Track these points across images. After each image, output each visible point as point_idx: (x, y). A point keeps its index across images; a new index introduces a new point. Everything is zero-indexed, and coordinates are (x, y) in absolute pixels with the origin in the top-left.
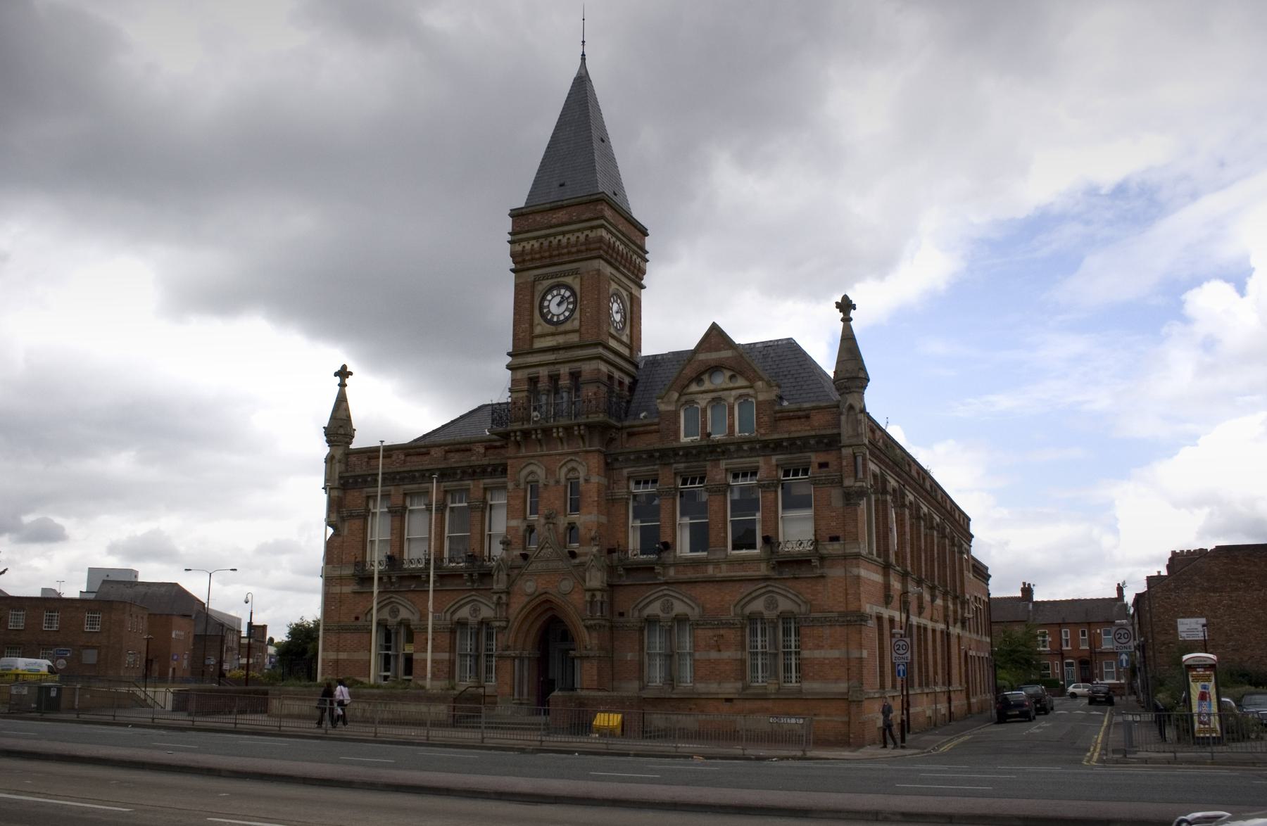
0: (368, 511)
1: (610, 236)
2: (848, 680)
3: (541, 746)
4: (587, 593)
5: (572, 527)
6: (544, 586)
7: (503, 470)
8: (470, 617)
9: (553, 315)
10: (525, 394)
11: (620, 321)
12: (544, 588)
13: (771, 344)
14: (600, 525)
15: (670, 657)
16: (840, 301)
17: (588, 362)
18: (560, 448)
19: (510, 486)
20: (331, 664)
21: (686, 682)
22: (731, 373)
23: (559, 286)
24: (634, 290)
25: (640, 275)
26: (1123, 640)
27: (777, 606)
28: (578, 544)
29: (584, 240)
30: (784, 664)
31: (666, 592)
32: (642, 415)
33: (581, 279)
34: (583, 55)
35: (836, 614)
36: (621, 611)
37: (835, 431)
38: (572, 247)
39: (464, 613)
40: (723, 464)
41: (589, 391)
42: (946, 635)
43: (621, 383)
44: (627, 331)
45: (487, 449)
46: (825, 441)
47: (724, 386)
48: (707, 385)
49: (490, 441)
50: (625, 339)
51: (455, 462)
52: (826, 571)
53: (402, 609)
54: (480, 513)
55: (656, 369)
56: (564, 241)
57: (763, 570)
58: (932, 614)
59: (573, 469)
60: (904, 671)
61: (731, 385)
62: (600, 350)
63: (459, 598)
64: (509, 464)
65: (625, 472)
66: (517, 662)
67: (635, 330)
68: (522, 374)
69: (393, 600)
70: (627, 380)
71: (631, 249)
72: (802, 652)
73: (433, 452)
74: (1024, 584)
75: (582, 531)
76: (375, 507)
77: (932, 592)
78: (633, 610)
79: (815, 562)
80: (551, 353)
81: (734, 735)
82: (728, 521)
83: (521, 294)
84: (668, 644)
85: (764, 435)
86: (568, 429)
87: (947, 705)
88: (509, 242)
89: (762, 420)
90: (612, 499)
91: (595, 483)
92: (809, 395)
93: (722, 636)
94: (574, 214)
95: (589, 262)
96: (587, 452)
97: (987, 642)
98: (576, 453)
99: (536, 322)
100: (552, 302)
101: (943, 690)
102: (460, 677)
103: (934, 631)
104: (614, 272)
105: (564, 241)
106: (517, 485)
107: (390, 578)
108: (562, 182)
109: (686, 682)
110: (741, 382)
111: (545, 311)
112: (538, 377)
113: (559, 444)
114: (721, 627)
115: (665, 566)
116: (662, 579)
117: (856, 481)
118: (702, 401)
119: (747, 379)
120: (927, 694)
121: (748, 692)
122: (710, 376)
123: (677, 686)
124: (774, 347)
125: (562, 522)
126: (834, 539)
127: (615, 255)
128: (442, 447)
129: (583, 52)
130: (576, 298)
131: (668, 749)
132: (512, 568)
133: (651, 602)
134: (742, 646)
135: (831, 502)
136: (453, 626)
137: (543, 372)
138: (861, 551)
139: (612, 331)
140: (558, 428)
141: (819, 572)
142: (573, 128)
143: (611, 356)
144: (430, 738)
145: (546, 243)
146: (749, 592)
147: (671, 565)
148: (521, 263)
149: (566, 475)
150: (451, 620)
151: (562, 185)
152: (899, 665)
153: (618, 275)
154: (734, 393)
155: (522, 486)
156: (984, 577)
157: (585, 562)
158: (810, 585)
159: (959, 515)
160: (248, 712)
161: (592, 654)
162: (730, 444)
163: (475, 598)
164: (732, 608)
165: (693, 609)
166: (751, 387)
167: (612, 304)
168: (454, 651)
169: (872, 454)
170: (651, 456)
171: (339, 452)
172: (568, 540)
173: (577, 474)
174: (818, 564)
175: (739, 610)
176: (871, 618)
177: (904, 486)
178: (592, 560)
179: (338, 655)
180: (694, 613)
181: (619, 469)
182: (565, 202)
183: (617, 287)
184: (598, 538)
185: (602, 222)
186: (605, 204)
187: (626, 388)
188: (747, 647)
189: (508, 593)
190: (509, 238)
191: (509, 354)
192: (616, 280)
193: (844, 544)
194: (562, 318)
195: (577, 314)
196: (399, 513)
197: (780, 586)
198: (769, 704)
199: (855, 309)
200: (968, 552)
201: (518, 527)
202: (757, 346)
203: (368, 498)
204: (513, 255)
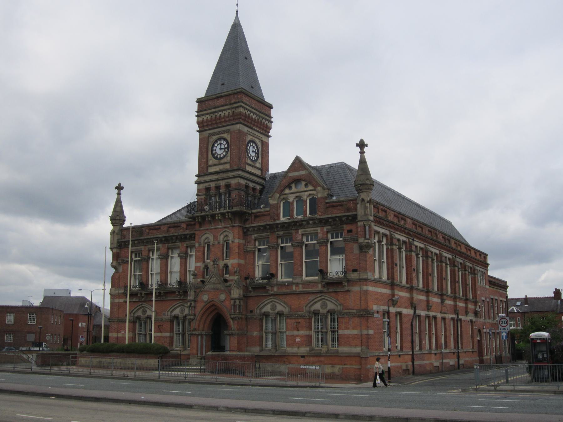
0: (149, 258)
3: (32, 371)
5: (226, 266)
6: (212, 297)
7: (192, 237)
8: (180, 314)
9: (218, 154)
11: (255, 156)
12: (212, 298)
13: (332, 165)
16: (359, 143)
17: (234, 179)
18: (220, 225)
19: (197, 245)
20: (114, 339)
22: (306, 183)
23: (221, 139)
24: (264, 138)
25: (268, 130)
26: (504, 325)
27: (327, 306)
28: (228, 275)
29: (232, 114)
31: (273, 300)
32: (262, 206)
33: (231, 135)
34: (237, 12)
35: (355, 311)
36: (251, 310)
37: (354, 213)
38: (226, 118)
39: (177, 312)
40: (300, 232)
41: (234, 194)
42: (457, 322)
43: (254, 189)
44: (260, 160)
45: (187, 225)
46: (350, 218)
47: (302, 190)
48: (294, 189)
55: (275, 180)
56: (223, 115)
57: (320, 287)
59: (227, 236)
61: (305, 189)
62: (240, 173)
63: (174, 304)
64: (196, 234)
65: (253, 236)
66: (199, 337)
67: (264, 160)
68: (202, 186)
69: (143, 305)
70: (258, 187)
71: (260, 117)
72: (339, 331)
74: (556, 289)
75: (230, 267)
76: (153, 255)
78: (257, 309)
80: (216, 175)
81: (306, 375)
84: (274, 327)
86: (223, 215)
87: (456, 360)
88: (196, 116)
90: (247, 251)
91: (237, 243)
92: (346, 193)
93: (300, 322)
94: (228, 100)
96: (233, 227)
98: (228, 227)
100: (217, 147)
101: (453, 351)
102: (176, 345)
103: (444, 319)
104: (249, 130)
105: (223, 115)
106: (200, 245)
107: (141, 294)
108: (223, 82)
111: (214, 152)
113: (220, 223)
114: (299, 318)
115: (272, 286)
116: (270, 293)
117: (365, 240)
119: (313, 185)
120: (435, 354)
123: (279, 349)
124: (333, 167)
125: (221, 263)
126: (355, 271)
128: (166, 225)
129: (237, 10)
130: (229, 145)
131: (246, 381)
132: (197, 288)
133: (266, 305)
136: (172, 319)
137: (213, 185)
139: (249, 162)
141: (347, 288)
142: (230, 53)
143: (247, 175)
144: (136, 376)
145: (214, 116)
146: (312, 299)
147: (275, 285)
148: (203, 126)
149: (223, 239)
150: (171, 316)
151: (223, 84)
153: (252, 131)
154: (307, 193)
155: (202, 245)
156: (503, 288)
157: (231, 285)
160: (186, 365)
161: (234, 332)
164: (304, 308)
165: (285, 308)
166: (315, 190)
167: (249, 147)
168: (173, 332)
170: (264, 228)
171: (118, 228)
172: (224, 272)
173: (228, 239)
175: (308, 308)
178: (234, 284)
179: (117, 335)
180: (286, 310)
181: (250, 235)
182: (223, 94)
184: (238, 272)
186: (242, 94)
187: (258, 192)
188: (313, 328)
189: (195, 301)
190: (196, 114)
191: (196, 176)
192: (252, 134)
193: (360, 273)
194: (222, 156)
195: (229, 154)
196: (164, 258)
198: (322, 359)
200: (485, 273)
202: (325, 167)
203: (149, 251)
204: (198, 123)
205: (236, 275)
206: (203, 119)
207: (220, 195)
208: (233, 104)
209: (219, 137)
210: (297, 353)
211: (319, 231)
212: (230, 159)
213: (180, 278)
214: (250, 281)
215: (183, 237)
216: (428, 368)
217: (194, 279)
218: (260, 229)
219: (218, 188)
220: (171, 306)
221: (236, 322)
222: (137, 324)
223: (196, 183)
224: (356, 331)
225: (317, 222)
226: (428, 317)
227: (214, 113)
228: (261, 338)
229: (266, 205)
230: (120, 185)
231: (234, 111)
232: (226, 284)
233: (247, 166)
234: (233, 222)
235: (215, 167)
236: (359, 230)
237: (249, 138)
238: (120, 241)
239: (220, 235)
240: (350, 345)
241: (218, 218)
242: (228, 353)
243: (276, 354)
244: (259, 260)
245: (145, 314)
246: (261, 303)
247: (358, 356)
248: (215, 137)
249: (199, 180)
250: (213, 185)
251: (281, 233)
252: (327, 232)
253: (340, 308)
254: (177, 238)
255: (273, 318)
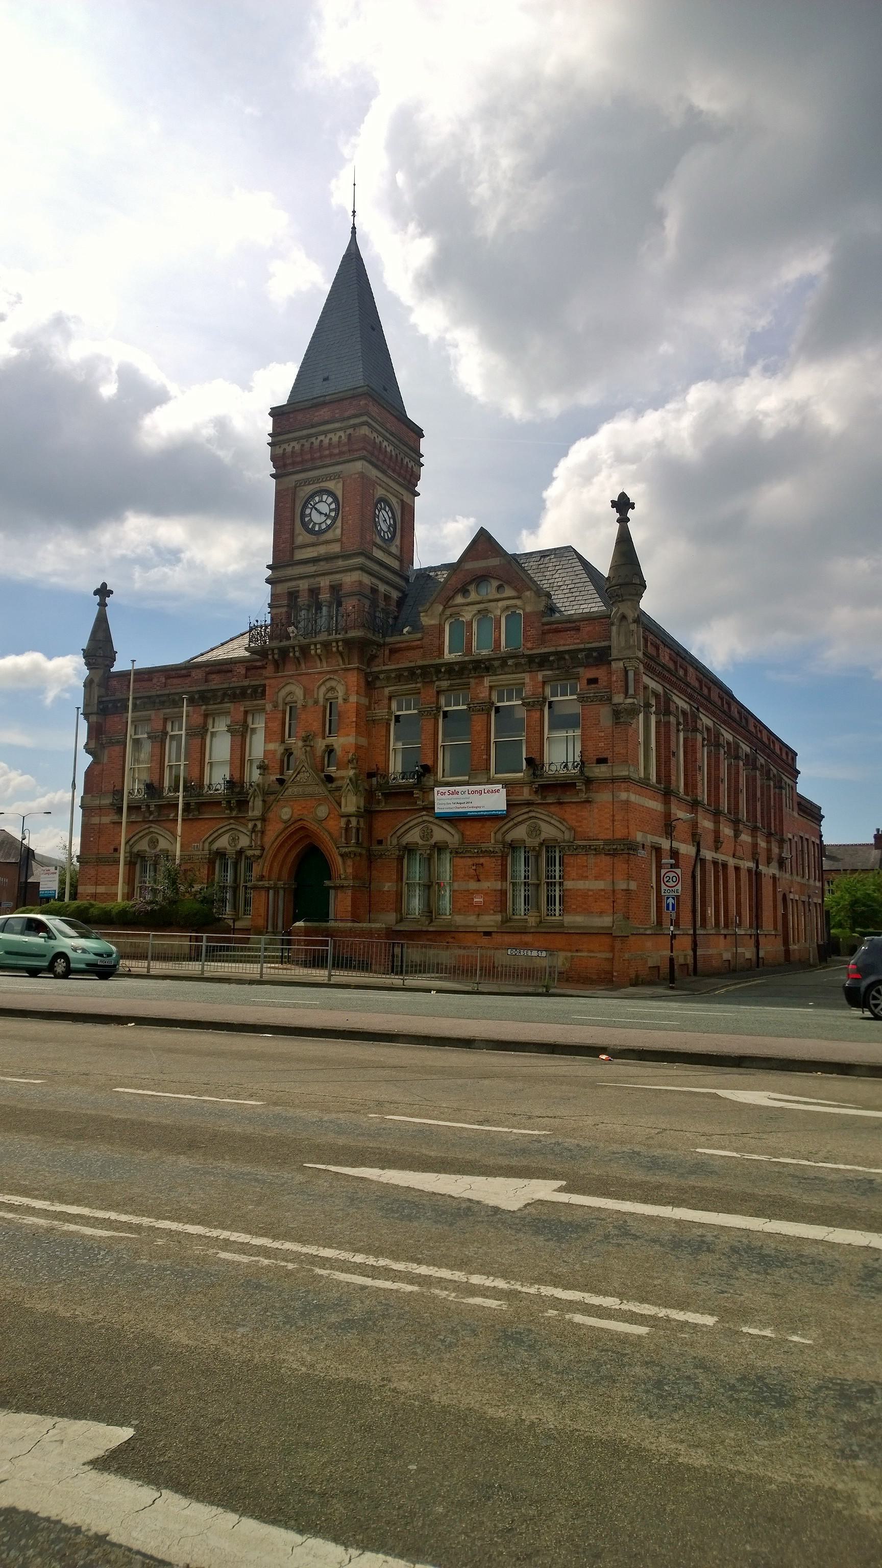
1: (375, 435)
2: (614, 913)
4: (342, 819)
5: (330, 750)
8: (228, 847)
10: (284, 610)
14: (358, 747)
15: (430, 887)
19: (269, 707)
21: (446, 915)
24: (406, 497)
25: (413, 481)
29: (346, 440)
30: (548, 895)
34: (354, 228)
35: (601, 843)
39: (223, 842)
40: (487, 682)
41: (350, 604)
42: (756, 876)
43: (387, 598)
44: (397, 541)
45: (248, 669)
46: (595, 654)
47: (491, 597)
48: (473, 596)
49: (248, 661)
50: (394, 550)
51: (215, 684)
52: (593, 795)
53: (161, 839)
54: (240, 737)
58: (735, 850)
60: (673, 905)
61: (499, 596)
62: (360, 560)
65: (387, 691)
68: (283, 588)
69: (152, 830)
70: (395, 595)
72: (565, 883)
73: (193, 674)
77: (735, 827)
79: (580, 786)
80: (312, 565)
82: (492, 742)
83: (282, 502)
85: (531, 649)
86: (326, 645)
87: (754, 950)
89: (529, 633)
90: (374, 721)
93: (482, 864)
95: (351, 465)
97: (817, 888)
99: (297, 531)
101: (749, 932)
103: (737, 869)
104: (380, 475)
105: (326, 441)
107: (148, 806)
108: (326, 375)
109: (446, 915)
110: (509, 592)
111: (307, 519)
112: (298, 591)
118: (467, 615)
119: (517, 590)
120: (725, 936)
121: (509, 924)
122: (477, 586)
125: (320, 744)
126: (602, 761)
127: (381, 457)
129: (354, 224)
133: (410, 828)
134: (503, 877)
135: (599, 721)
137: (304, 585)
138: (631, 774)
139: (378, 541)
140: (315, 645)
141: (583, 796)
143: (376, 568)
145: (307, 445)
150: (210, 850)
152: (668, 898)
154: (501, 604)
156: (817, 819)
157: (342, 787)
158: (574, 811)
159: (781, 749)
161: (345, 883)
162: (494, 659)
163: (233, 826)
164: (492, 834)
166: (519, 598)
169: (647, 667)
170: (411, 674)
172: (326, 762)
174: (583, 788)
176: (643, 848)
177: (698, 709)
181: (379, 688)
182: (327, 398)
183: (384, 492)
184: (355, 761)
185: (365, 418)
187: (394, 603)
190: (270, 439)
191: (269, 567)
192: (383, 484)
194: (324, 526)
197: (544, 812)
198: (528, 938)
199: (633, 508)
200: (793, 788)
201: (276, 751)
204: (273, 458)
205: (352, 768)
206: (285, 449)
207: (319, 607)
208: (349, 418)
209: (318, 489)
210: (476, 927)
211: (527, 680)
212: (342, 532)
213: (231, 775)
214: (379, 780)
215: (238, 692)
216: (715, 963)
217: (261, 777)
218: (398, 677)
219: (314, 592)
220: (212, 832)
221: (349, 862)
222: (138, 867)
223: (268, 581)
224: (602, 882)
225: (523, 661)
226: (715, 863)
227: (309, 436)
228: (399, 895)
229: (413, 629)
230: (104, 585)
231: (350, 434)
232: (330, 785)
233: (374, 548)
234: (347, 661)
235: (309, 549)
236: (614, 679)
237: (380, 492)
238: (104, 699)
239: (319, 687)
240: (588, 912)
241: (316, 652)
242: (332, 924)
243: (431, 929)
244: (397, 739)
245: (155, 847)
246: (401, 825)
247: (607, 933)
248: (309, 489)
249: (276, 576)
250: (304, 585)
251: (445, 684)
252: (544, 683)
253: (568, 836)
254: (225, 695)
255: (425, 856)
